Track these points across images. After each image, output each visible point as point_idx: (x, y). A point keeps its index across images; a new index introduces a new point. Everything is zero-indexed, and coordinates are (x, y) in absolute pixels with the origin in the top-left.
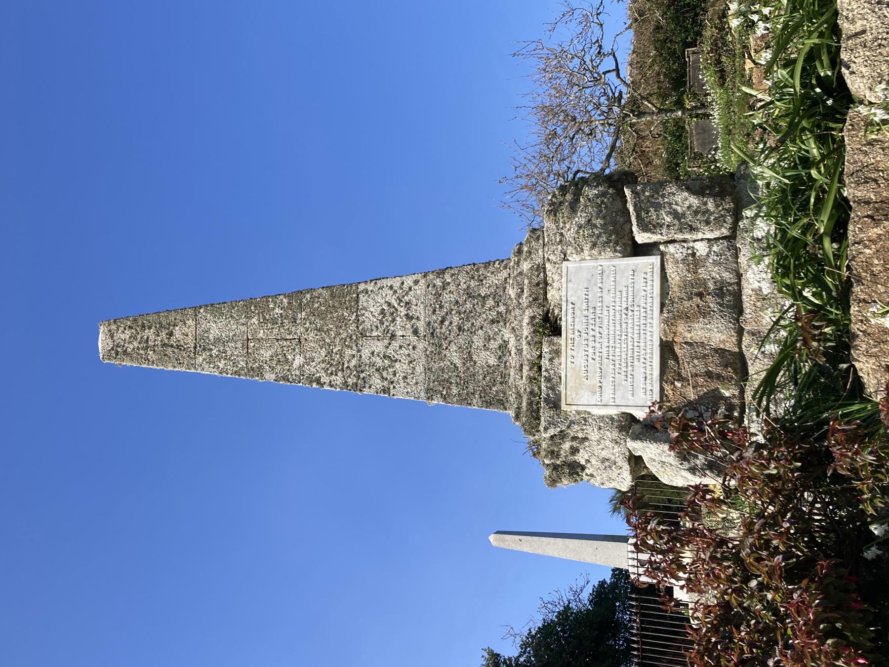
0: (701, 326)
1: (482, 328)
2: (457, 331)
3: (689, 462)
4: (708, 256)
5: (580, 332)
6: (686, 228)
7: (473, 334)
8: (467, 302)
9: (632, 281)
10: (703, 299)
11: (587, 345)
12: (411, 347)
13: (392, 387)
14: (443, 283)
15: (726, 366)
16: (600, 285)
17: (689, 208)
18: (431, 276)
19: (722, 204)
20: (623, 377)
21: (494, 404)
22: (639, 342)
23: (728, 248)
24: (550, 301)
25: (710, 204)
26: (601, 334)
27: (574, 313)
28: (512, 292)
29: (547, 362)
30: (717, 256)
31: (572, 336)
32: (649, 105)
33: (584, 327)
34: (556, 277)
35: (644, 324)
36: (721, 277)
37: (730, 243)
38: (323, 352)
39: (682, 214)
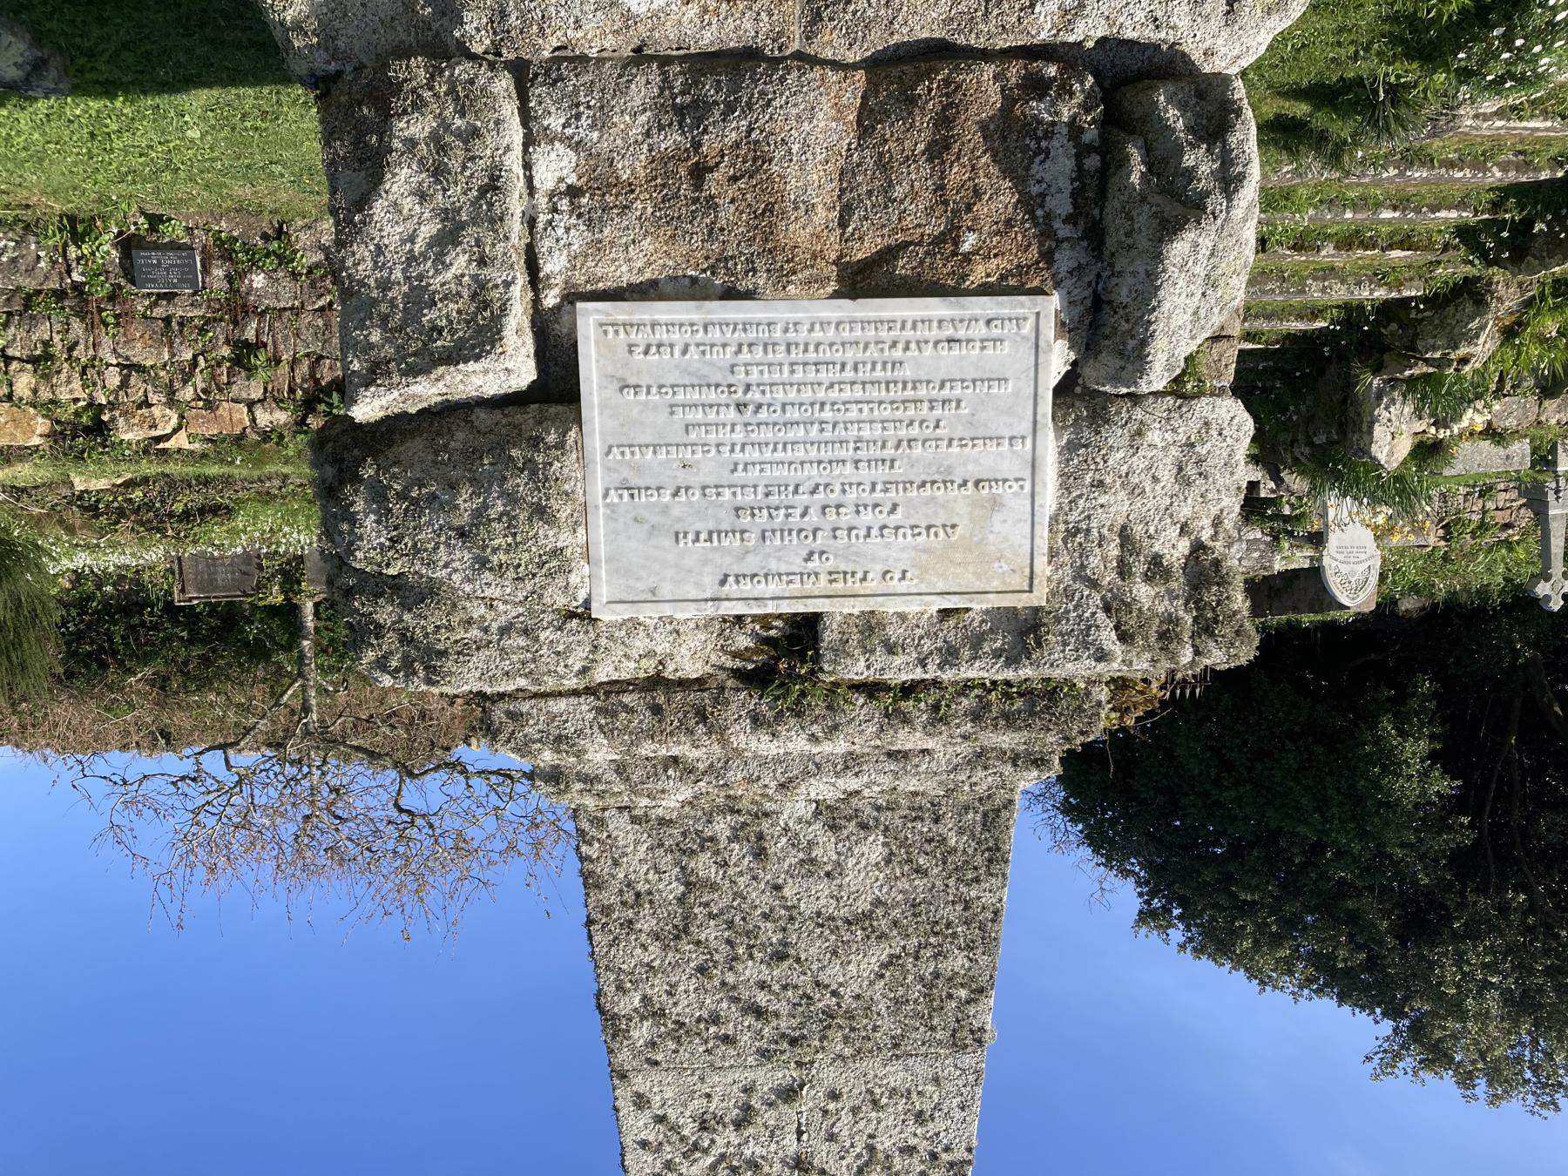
0: (793, 170)
1: (778, 888)
2: (786, 964)
3: (1208, 194)
4: (578, 143)
5: (811, 554)
6: (490, 205)
7: (795, 913)
8: (703, 937)
9: (654, 390)
10: (712, 163)
11: (850, 529)
12: (832, 1106)
13: (945, 1157)
14: (643, 1018)
15: (912, 101)
16: (667, 497)
17: (422, 196)
18: (624, 1057)
19: (414, 91)
20: (949, 413)
21: (997, 840)
22: (843, 366)
23: (555, 82)
24: (708, 669)
25: (413, 130)
26: (817, 486)
27: (753, 576)
28: (675, 797)
29: (898, 661)
30: (578, 117)
31: (823, 578)
32: (290, 692)
33: (795, 541)
34: (640, 643)
35: (788, 351)
36: (645, 110)
37: (540, 79)
39: (442, 221)
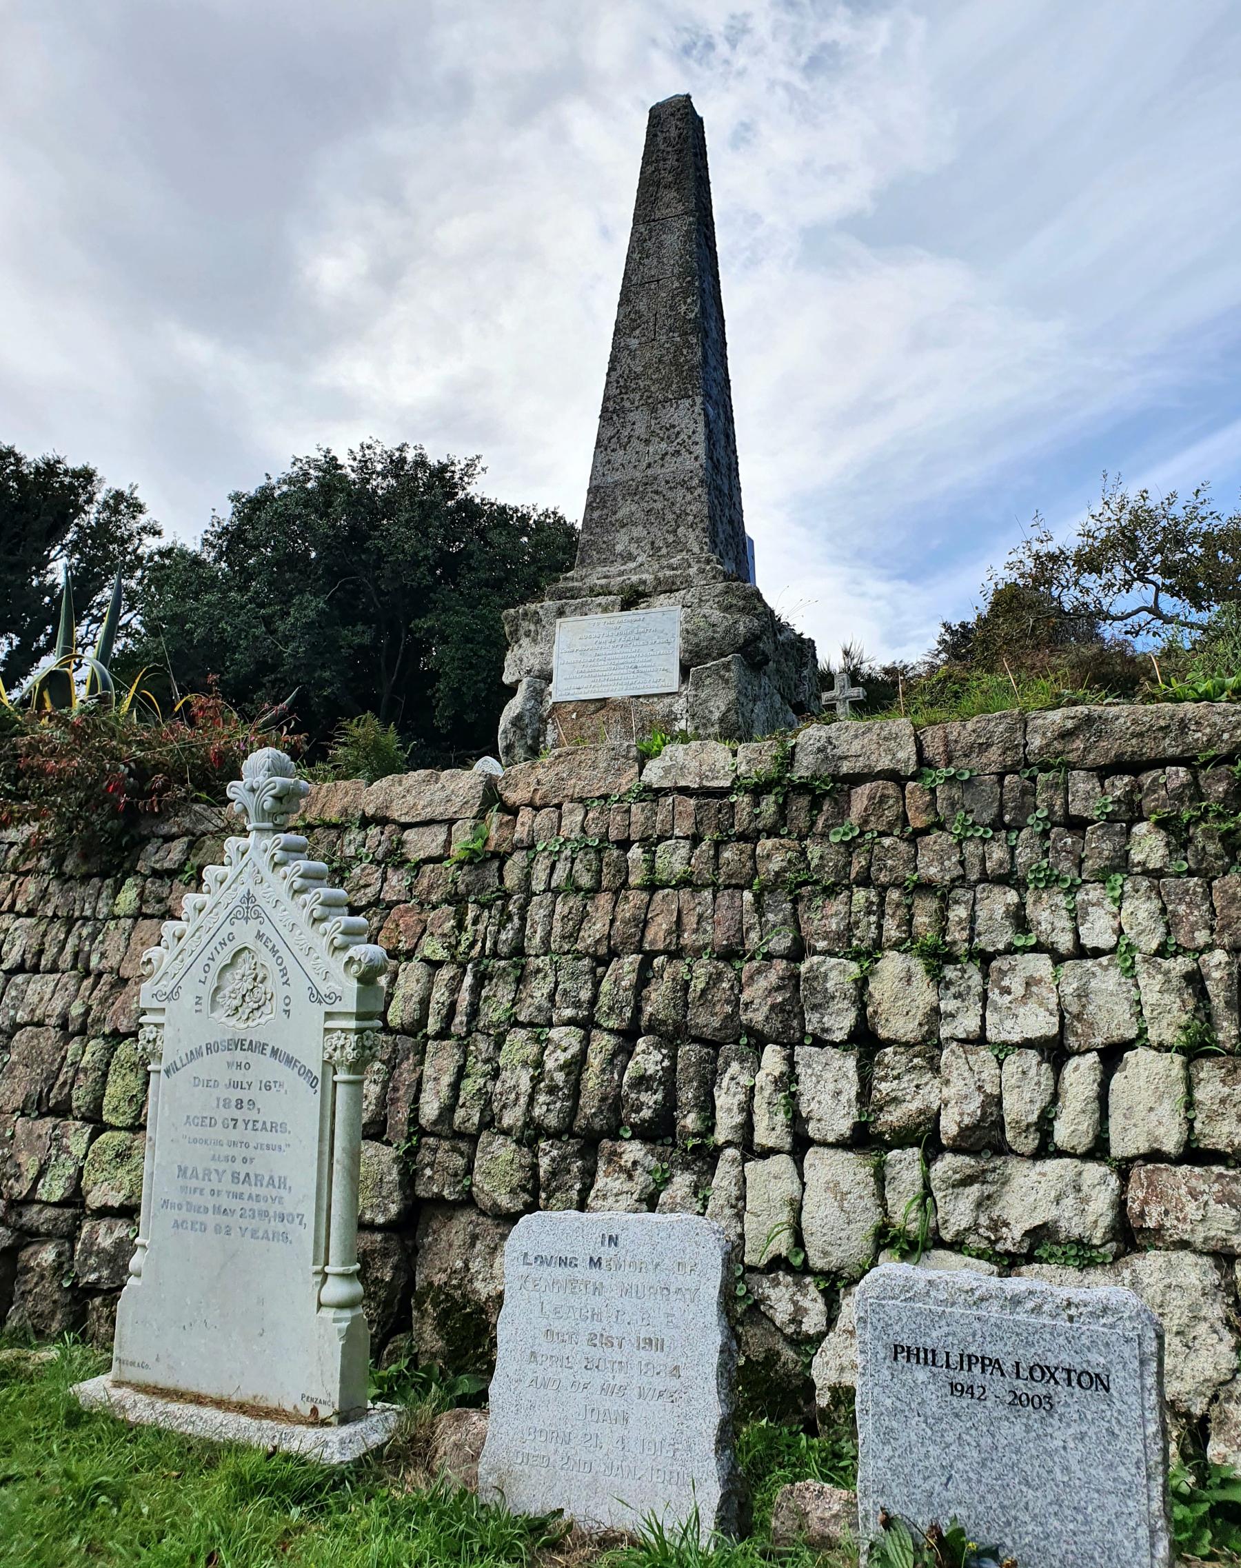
38: (639, 369)
